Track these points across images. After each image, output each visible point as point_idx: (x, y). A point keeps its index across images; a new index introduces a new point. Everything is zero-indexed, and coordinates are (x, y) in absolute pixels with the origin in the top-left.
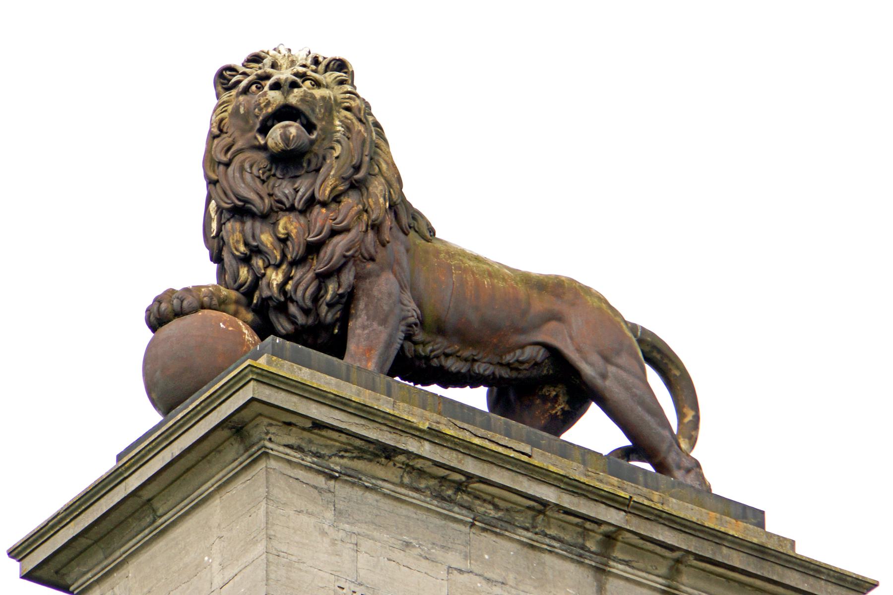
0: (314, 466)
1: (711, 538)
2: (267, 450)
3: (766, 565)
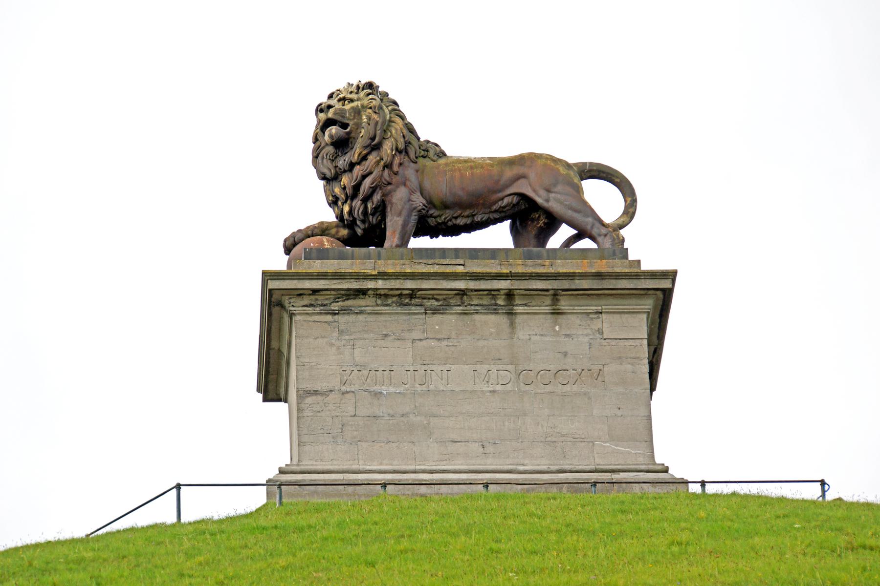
1: (567, 278)
2: (292, 312)
3: (604, 281)
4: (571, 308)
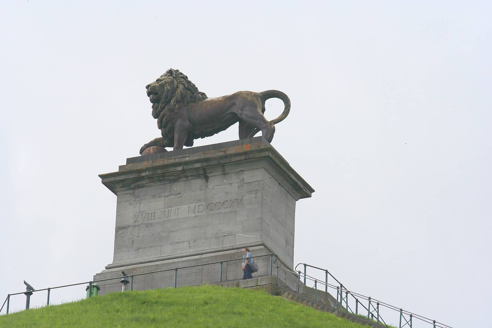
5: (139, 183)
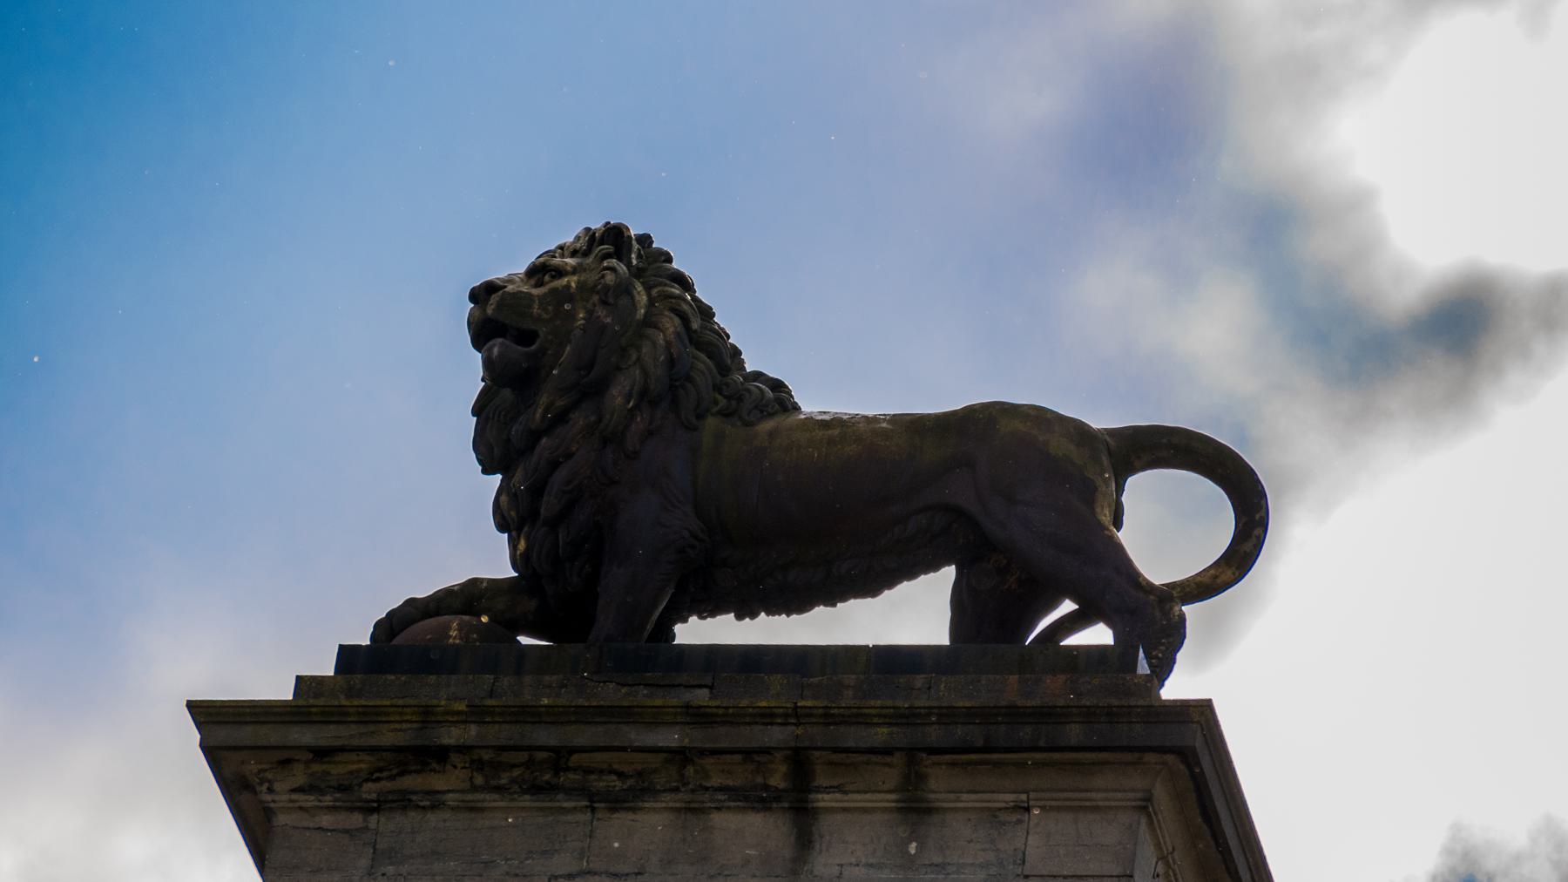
0: (337, 804)
4: (952, 796)
5: (408, 782)
